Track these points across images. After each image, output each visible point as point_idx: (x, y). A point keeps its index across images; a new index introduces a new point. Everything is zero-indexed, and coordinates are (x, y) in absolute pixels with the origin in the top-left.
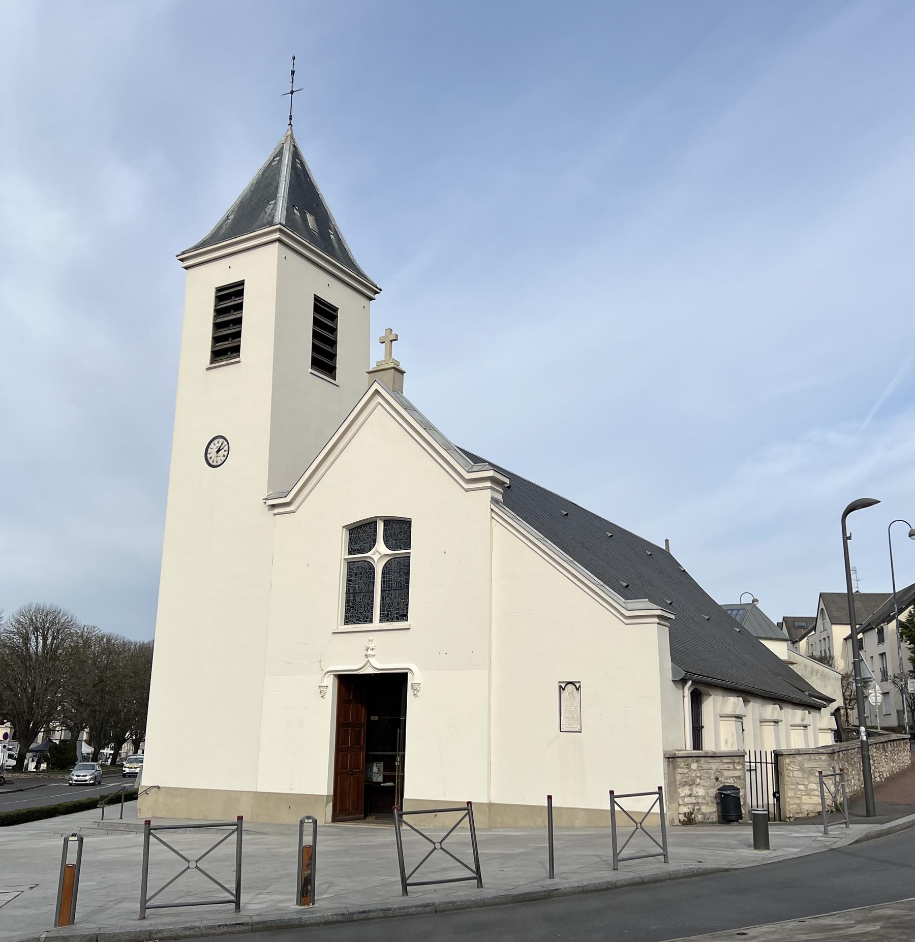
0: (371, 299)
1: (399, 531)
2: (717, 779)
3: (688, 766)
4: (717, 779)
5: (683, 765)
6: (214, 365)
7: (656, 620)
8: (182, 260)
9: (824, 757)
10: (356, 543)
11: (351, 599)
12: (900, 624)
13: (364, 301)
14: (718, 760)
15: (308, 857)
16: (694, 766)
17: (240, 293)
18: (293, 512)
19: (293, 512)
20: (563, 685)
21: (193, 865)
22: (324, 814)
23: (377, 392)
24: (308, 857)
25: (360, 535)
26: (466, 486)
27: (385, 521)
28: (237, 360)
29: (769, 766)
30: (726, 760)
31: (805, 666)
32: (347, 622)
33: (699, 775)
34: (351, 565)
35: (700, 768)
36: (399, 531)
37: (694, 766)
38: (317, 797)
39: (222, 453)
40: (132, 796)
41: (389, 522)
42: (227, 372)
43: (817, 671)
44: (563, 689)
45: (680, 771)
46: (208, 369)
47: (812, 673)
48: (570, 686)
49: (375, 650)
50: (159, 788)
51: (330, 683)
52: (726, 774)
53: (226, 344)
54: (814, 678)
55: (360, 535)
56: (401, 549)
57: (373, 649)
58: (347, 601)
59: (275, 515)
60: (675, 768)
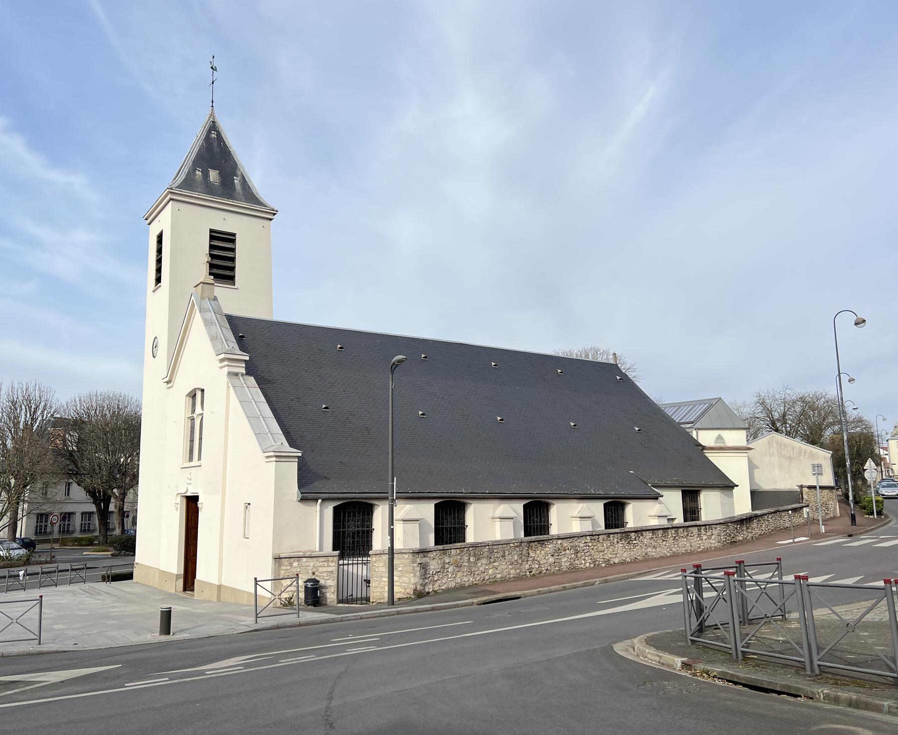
0: (271, 220)
2: (314, 573)
3: (291, 564)
4: (314, 573)
5: (286, 563)
7: (274, 459)
9: (406, 556)
13: (268, 222)
14: (315, 559)
15: (167, 616)
16: (296, 564)
21: (15, 621)
24: (167, 616)
29: (796, 540)
30: (321, 559)
31: (793, 448)
33: (447, 561)
35: (300, 566)
37: (296, 564)
40: (129, 576)
43: (805, 452)
45: (284, 568)
47: (800, 453)
52: (321, 569)
54: (802, 457)
60: (280, 566)
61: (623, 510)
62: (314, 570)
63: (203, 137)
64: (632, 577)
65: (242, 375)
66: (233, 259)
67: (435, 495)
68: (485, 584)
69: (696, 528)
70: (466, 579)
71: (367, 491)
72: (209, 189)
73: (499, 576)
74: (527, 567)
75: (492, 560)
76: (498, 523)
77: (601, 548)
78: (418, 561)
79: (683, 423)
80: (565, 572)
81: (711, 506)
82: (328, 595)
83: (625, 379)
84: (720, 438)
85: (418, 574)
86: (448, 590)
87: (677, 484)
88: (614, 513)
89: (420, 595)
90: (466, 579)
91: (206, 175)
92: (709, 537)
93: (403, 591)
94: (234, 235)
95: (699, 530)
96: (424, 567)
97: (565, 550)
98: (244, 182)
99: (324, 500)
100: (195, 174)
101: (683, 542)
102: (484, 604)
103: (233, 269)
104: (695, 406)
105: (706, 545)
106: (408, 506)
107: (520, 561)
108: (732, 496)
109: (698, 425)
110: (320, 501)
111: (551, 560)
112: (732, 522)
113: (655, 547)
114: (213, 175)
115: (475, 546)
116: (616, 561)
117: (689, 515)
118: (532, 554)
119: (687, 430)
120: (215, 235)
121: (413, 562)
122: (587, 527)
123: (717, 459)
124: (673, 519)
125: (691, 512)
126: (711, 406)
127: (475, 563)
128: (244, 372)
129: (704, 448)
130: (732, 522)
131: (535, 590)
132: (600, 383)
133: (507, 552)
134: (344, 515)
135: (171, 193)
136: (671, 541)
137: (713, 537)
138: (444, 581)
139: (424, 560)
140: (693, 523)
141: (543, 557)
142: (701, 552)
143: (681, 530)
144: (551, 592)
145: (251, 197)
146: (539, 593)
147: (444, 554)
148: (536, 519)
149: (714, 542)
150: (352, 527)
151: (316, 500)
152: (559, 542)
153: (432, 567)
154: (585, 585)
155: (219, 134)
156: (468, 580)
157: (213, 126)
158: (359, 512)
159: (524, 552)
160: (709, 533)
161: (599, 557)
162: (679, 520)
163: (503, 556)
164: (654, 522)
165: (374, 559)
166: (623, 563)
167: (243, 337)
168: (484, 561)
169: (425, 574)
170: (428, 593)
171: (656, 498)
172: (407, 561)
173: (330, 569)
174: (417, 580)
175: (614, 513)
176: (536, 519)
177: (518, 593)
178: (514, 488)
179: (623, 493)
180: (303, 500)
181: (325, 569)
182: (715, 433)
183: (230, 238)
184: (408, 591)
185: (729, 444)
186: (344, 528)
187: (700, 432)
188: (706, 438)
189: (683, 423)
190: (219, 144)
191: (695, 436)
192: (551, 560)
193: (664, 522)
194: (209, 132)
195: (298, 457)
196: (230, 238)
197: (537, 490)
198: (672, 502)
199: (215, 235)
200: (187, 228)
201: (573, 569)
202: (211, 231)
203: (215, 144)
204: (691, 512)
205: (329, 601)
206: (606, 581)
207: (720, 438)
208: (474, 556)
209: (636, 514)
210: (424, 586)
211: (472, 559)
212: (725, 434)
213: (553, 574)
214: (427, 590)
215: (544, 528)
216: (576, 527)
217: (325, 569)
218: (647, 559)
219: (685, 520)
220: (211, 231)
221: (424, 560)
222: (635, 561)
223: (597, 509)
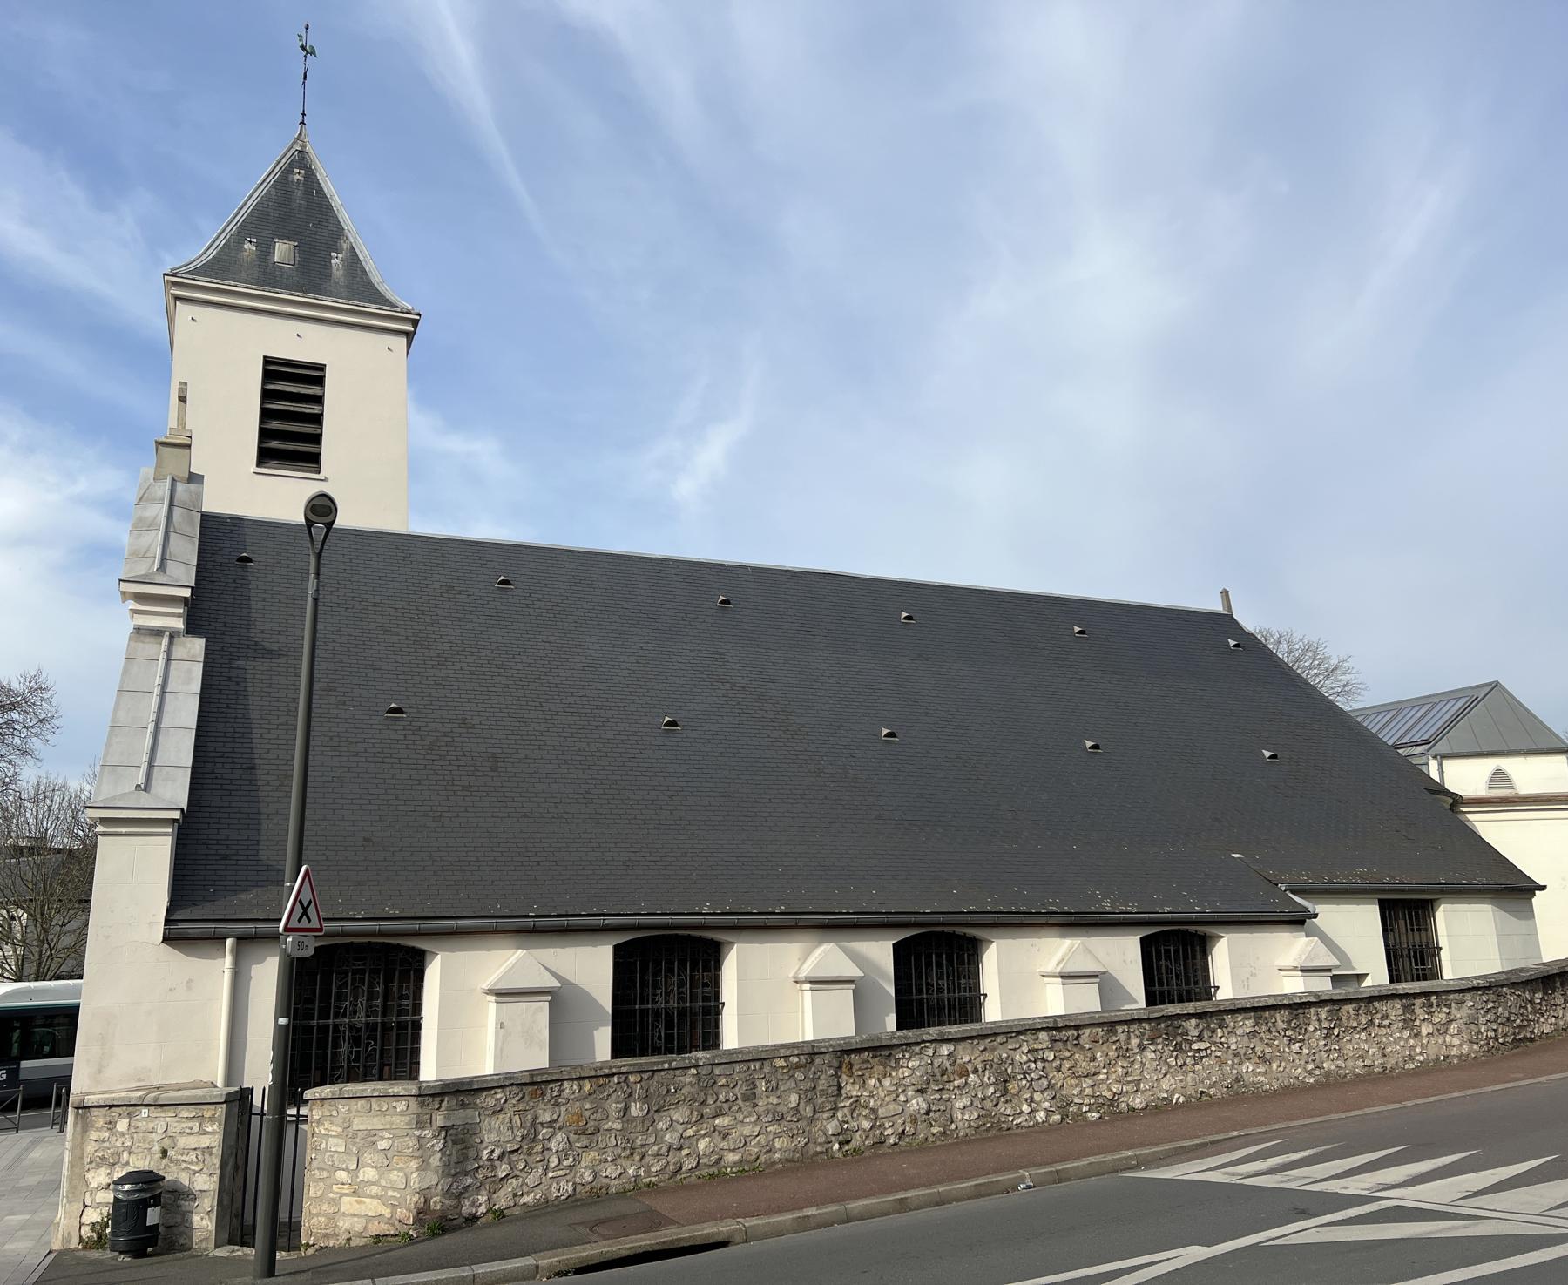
2: (164, 1153)
3: (111, 1124)
4: (164, 1153)
14: (170, 1112)
30: (185, 1113)
37: (122, 1125)
52: (182, 1142)
61: (1205, 954)
62: (167, 1143)
63: (272, 180)
64: (1150, 1162)
65: (173, 635)
66: (317, 419)
67: (609, 921)
68: (683, 1187)
69: (1398, 1004)
70: (611, 1171)
71: (811, 909)
72: (268, 276)
73: (732, 1157)
74: (832, 1127)
75: (707, 1111)
76: (807, 995)
77: (1084, 1066)
78: (439, 1119)
79: (1406, 745)
80: (966, 1141)
81: (1468, 940)
82: (196, 1218)
83: (1251, 646)
84: (1499, 776)
85: (435, 1161)
86: (547, 1207)
87: (1363, 884)
88: (1175, 961)
89: (440, 1226)
90: (611, 1171)
91: (265, 250)
92: (1442, 1029)
93: (387, 1212)
94: (322, 368)
95: (1408, 1009)
96: (460, 1141)
97: (964, 1073)
98: (354, 262)
99: (242, 939)
100: (239, 248)
101: (1355, 1043)
102: (579, 1271)
103: (316, 439)
104: (1436, 704)
105: (1432, 1051)
106: (1068, 942)
107: (808, 1111)
108: (1530, 915)
109: (1441, 747)
110: (229, 942)
111: (917, 1104)
112: (1513, 985)
113: (1263, 1059)
114: (282, 251)
115: (738, 1059)
116: (1138, 1102)
117: (1404, 965)
118: (851, 1089)
119: (1415, 761)
120: (274, 370)
121: (420, 1125)
122: (1087, 1001)
123: (1496, 830)
124: (1360, 977)
125: (1411, 953)
126: (1475, 701)
127: (649, 1121)
128: (179, 624)
129: (1457, 801)
130: (1513, 985)
131: (789, 1216)
132: (1205, 658)
133: (762, 1086)
134: (918, 960)
135: (175, 284)
136: (1317, 1040)
137: (1453, 1028)
138: (531, 1179)
139: (460, 1117)
140: (1190, 1007)
141: (689, 1135)
142: (1416, 1073)
143: (1350, 1008)
144: (848, 1219)
145: (361, 288)
146: (803, 1225)
147: (534, 1096)
148: (935, 979)
149: (1456, 1043)
150: (667, 998)
151: (221, 939)
152: (945, 1050)
153: (489, 1137)
154: (978, 1193)
155: (310, 175)
156: (616, 1172)
157: (300, 160)
158: (682, 964)
159: (823, 1084)
160: (1440, 1017)
161: (1079, 1093)
162: (1377, 975)
163: (750, 1097)
164: (1295, 986)
165: (316, 1114)
166: (1160, 1108)
167: (248, 560)
168: (679, 1115)
169: (463, 1158)
170: (472, 1219)
171: (1299, 921)
172: (400, 1122)
173: (205, 1141)
174: (432, 1179)
175: (1175, 961)
176: (935, 979)
177: (709, 1230)
178: (873, 900)
179: (1197, 907)
180: (165, 940)
181: (192, 1142)
182: (1488, 765)
183: (313, 375)
184: (402, 1213)
185: (1525, 788)
186: (324, 1014)
187: (1445, 762)
188: (1464, 777)
189: (1406, 745)
190: (308, 192)
191: (1434, 774)
192: (917, 1104)
193: (1323, 984)
194: (288, 171)
195: (175, 821)
196: (313, 375)
197: (936, 903)
198: (1356, 933)
199: (274, 370)
200: (226, 356)
201: (991, 1130)
202: (267, 361)
203: (299, 194)
204: (1411, 953)
205: (197, 1236)
206: (1059, 1178)
207: (1499, 776)
208: (646, 1098)
209: (1245, 965)
210: (459, 1196)
211: (635, 1110)
212: (1510, 765)
213: (924, 1146)
214: (466, 1209)
215: (702, 1022)
216: (1054, 1002)
217: (192, 1142)
218: (1239, 1095)
219: (1394, 977)
220: (267, 361)
221: (460, 1117)
222: (1199, 1102)
223: (1122, 956)
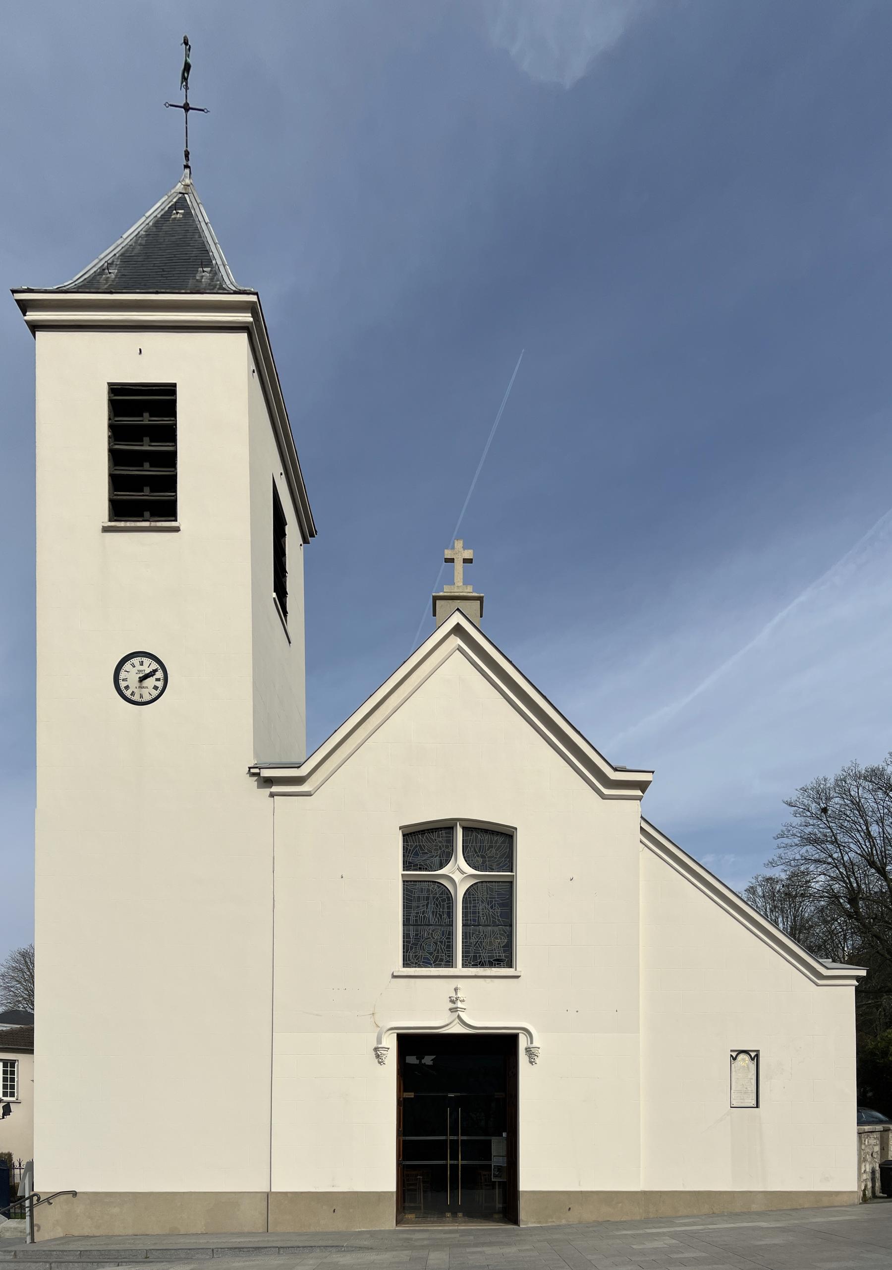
1: (493, 844)
6: (113, 524)
8: (24, 306)
10: (417, 854)
11: (412, 934)
12: (420, 1058)
17: (170, 409)
18: (308, 794)
19: (308, 794)
20: (734, 1054)
22: (388, 1220)
23: (458, 630)
25: (424, 843)
26: (606, 792)
27: (464, 828)
28: (173, 524)
32: (407, 963)
34: (409, 886)
36: (493, 844)
38: (380, 1196)
39: (150, 682)
41: (474, 829)
42: (142, 544)
44: (735, 1059)
46: (106, 530)
48: (742, 1056)
49: (461, 1002)
50: (74, 1194)
51: (391, 1043)
53: (143, 486)
55: (424, 843)
56: (492, 870)
57: (463, 1001)
58: (406, 936)
59: (272, 795)
